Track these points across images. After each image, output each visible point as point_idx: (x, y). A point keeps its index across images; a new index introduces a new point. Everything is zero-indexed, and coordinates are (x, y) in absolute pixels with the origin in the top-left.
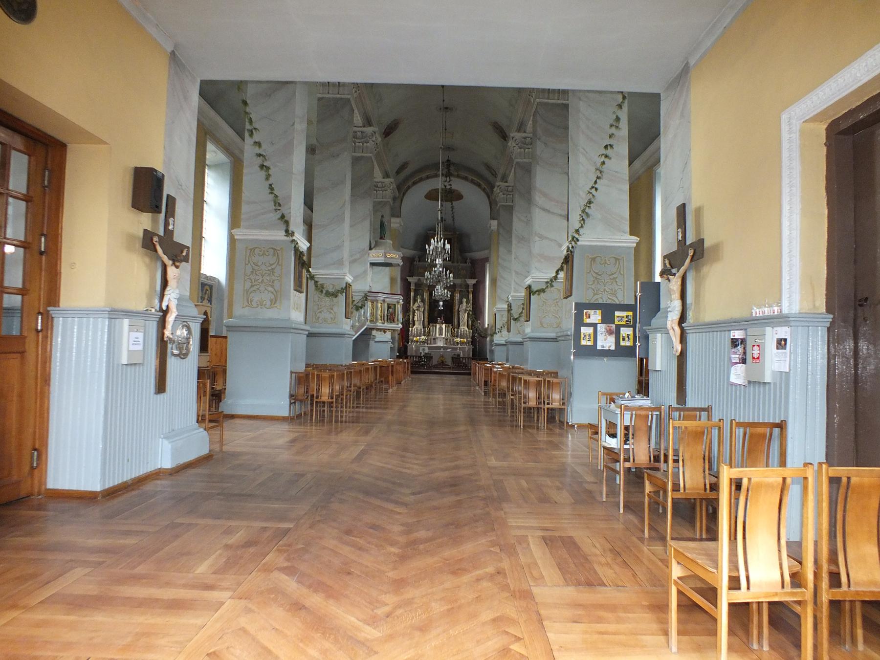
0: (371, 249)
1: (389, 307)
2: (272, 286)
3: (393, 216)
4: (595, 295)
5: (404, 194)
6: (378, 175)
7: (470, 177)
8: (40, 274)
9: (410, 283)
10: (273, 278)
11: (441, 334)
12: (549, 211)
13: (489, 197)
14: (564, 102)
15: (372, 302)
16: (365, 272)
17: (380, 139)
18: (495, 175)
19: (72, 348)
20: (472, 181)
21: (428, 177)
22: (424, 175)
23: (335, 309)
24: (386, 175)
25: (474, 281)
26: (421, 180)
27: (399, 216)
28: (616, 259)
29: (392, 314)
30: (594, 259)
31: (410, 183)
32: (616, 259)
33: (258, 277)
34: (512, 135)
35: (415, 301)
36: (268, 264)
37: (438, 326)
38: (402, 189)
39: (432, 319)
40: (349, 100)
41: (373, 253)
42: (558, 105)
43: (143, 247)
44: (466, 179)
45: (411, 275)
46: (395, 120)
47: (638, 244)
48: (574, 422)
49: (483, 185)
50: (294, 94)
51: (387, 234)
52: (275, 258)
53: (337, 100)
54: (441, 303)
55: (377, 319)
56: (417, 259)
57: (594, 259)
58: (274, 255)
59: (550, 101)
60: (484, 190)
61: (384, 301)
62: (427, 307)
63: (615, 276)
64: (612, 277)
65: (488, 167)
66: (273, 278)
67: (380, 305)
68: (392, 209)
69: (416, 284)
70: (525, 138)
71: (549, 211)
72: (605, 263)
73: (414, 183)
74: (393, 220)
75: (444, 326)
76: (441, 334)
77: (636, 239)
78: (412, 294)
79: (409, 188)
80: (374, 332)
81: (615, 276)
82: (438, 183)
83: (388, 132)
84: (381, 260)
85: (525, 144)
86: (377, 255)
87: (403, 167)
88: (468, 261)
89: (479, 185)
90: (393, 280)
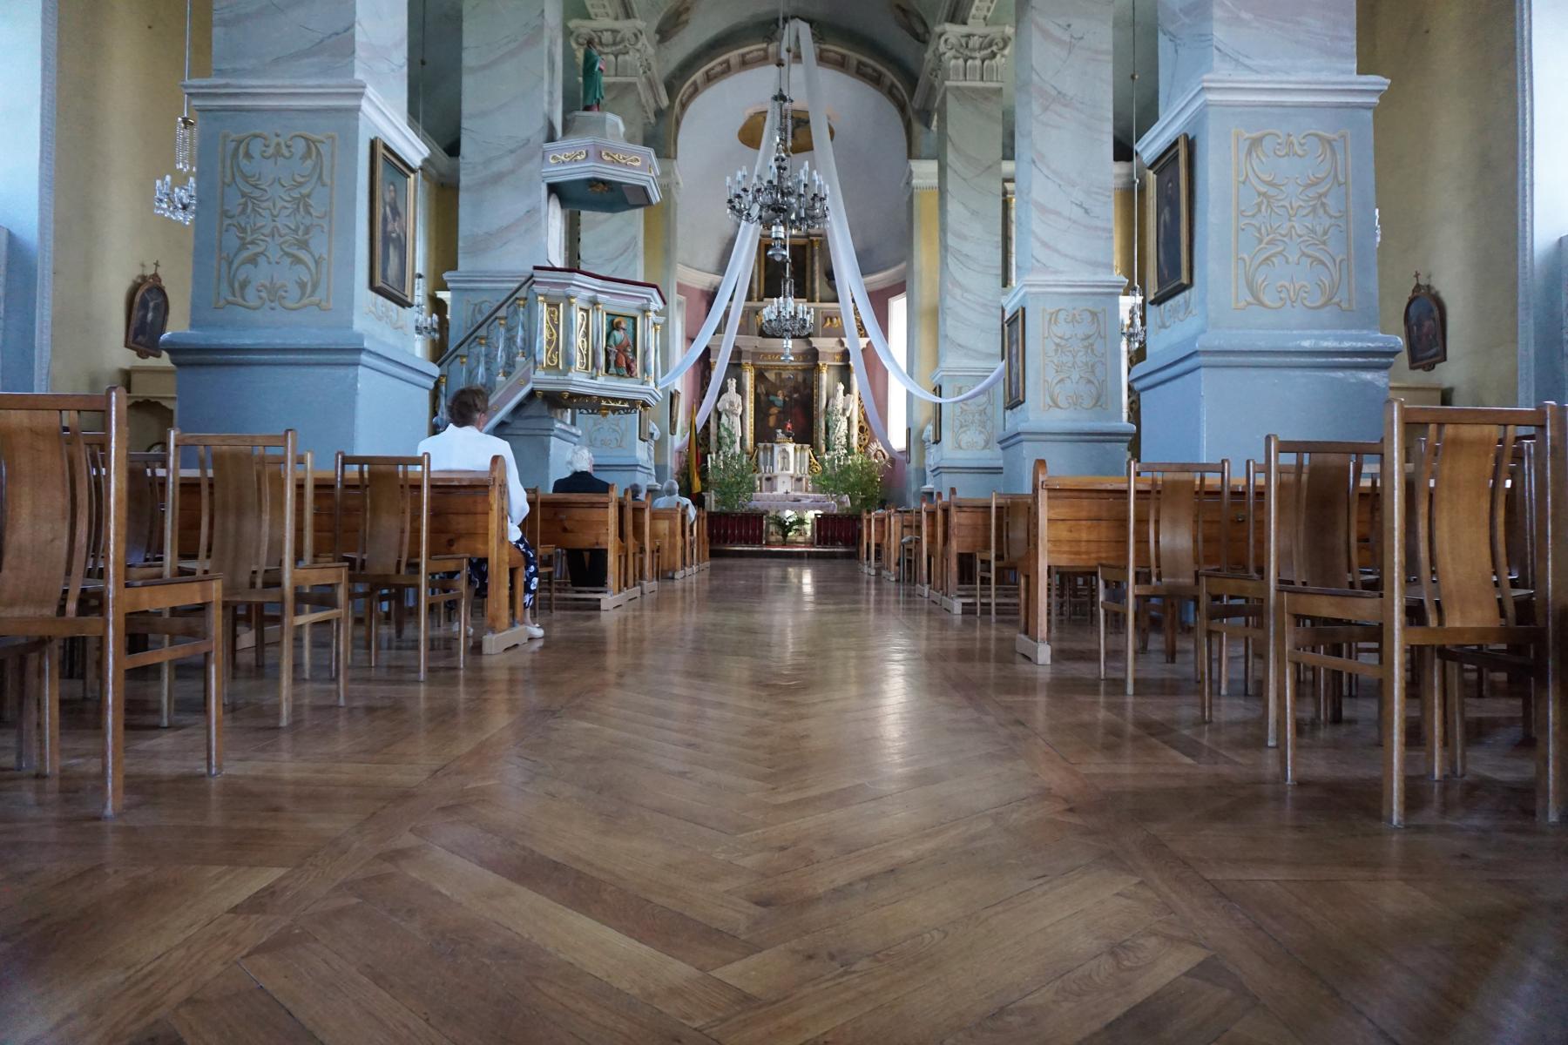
0: (551, 138)
1: (613, 326)
8: (260, 517)
11: (785, 467)
15: (553, 305)
16: (532, 212)
17: (651, 50)
26: (727, 70)
29: (622, 349)
34: (938, 29)
37: (777, 448)
41: (566, 147)
43: (127, 345)
47: (1384, 96)
48: (162, 606)
49: (890, 77)
55: (569, 362)
60: (891, 93)
61: (594, 303)
62: (750, 406)
67: (578, 317)
70: (969, 36)
73: (710, 79)
77: (1379, 82)
79: (695, 91)
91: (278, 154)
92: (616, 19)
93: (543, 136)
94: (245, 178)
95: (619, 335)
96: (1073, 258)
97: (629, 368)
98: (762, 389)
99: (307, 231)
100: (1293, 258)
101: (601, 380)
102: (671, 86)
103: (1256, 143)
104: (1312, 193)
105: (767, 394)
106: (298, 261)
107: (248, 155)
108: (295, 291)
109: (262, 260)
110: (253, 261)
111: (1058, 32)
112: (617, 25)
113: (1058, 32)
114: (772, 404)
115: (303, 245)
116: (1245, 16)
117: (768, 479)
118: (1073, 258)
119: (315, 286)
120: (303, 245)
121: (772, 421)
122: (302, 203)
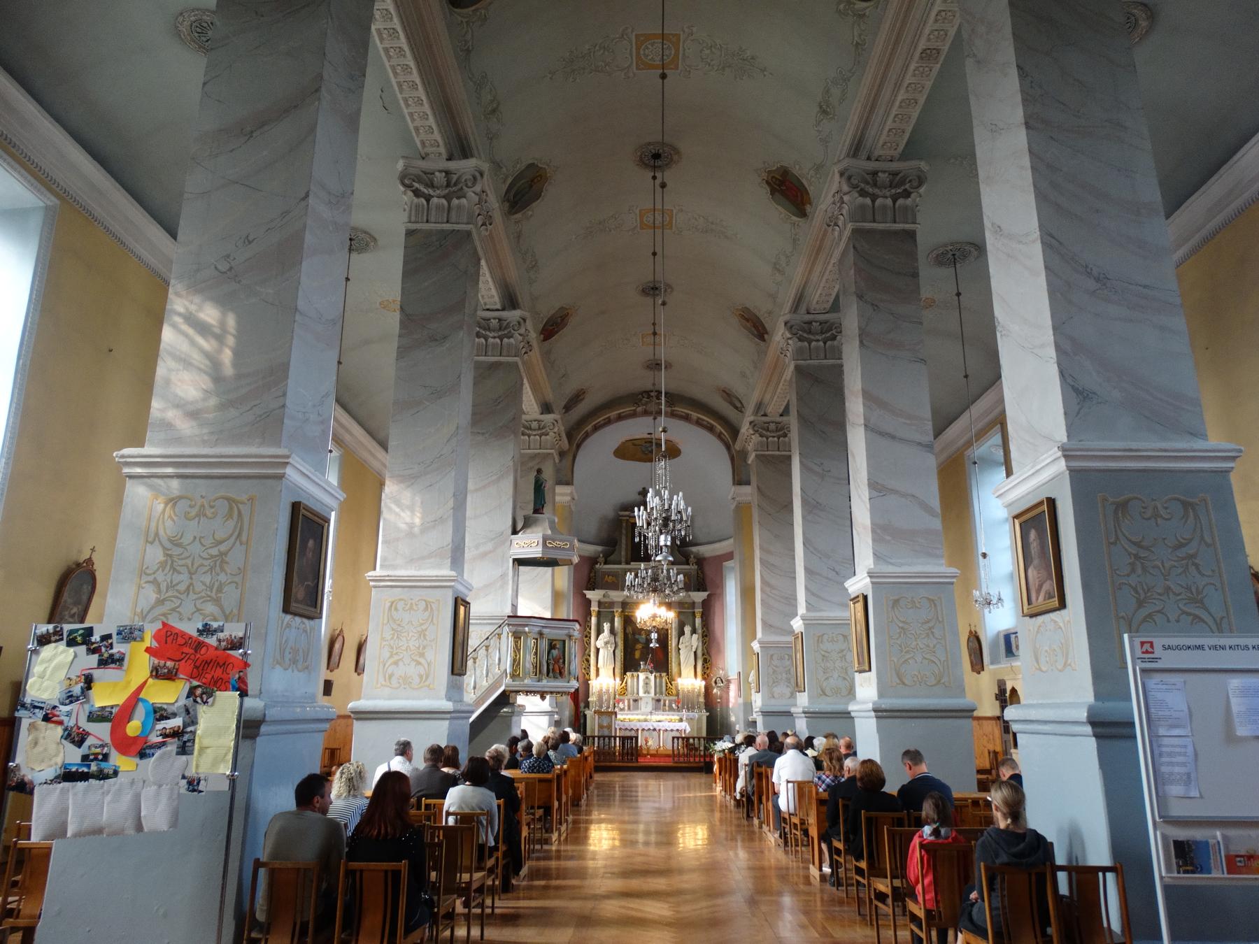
0: (515, 532)
1: (552, 646)
2: (217, 601)
3: (560, 483)
4: (1141, 604)
5: (579, 446)
6: (530, 404)
7: (695, 415)
9: (589, 602)
10: (222, 578)
12: (893, 437)
13: (728, 448)
14: (907, 226)
18: (740, 408)
19: (901, 565)
20: (699, 423)
21: (620, 418)
22: (613, 414)
23: (430, 655)
24: (546, 408)
25: (703, 595)
26: (609, 422)
27: (569, 483)
28: (1186, 505)
29: (556, 661)
30: (1122, 507)
31: (589, 428)
32: (1186, 505)
33: (177, 578)
35: (599, 631)
36: (208, 541)
38: (577, 435)
39: (629, 665)
40: (469, 234)
42: (896, 233)
44: (686, 418)
45: (592, 587)
46: (562, 308)
50: (312, 129)
51: (547, 509)
52: (231, 524)
53: (444, 235)
54: (654, 636)
56: (601, 559)
57: (1122, 507)
58: (229, 516)
59: (875, 225)
60: (720, 436)
61: (541, 634)
63: (1191, 549)
64: (1182, 553)
65: (728, 395)
66: (222, 578)
68: (558, 471)
69: (600, 604)
71: (893, 437)
72: (1156, 515)
73: (596, 428)
74: (559, 489)
75: (652, 677)
76: (647, 692)
78: (594, 620)
79: (587, 435)
80: (521, 700)
81: (1191, 549)
82: (637, 428)
83: (550, 330)
84: (536, 552)
85: (810, 332)
86: (529, 544)
87: (577, 398)
88: (692, 559)
89: (711, 429)
90: (557, 597)
91: (411, 608)
92: (449, 159)
93: (510, 531)
94: (394, 621)
95: (555, 652)
96: (920, 444)
97: (561, 674)
98: (629, 630)
99: (424, 648)
100: (919, 659)
101: (544, 682)
102: (570, 436)
103: (896, 602)
104: (926, 626)
105: (634, 634)
106: (419, 663)
107: (396, 609)
108: (417, 679)
109: (401, 663)
110: (396, 663)
111: (816, 468)
112: (452, 165)
113: (816, 468)
114: (637, 641)
115: (422, 655)
116: (888, 538)
117: (635, 701)
118: (920, 444)
119: (427, 677)
120: (422, 655)
121: (637, 654)
122: (422, 634)
